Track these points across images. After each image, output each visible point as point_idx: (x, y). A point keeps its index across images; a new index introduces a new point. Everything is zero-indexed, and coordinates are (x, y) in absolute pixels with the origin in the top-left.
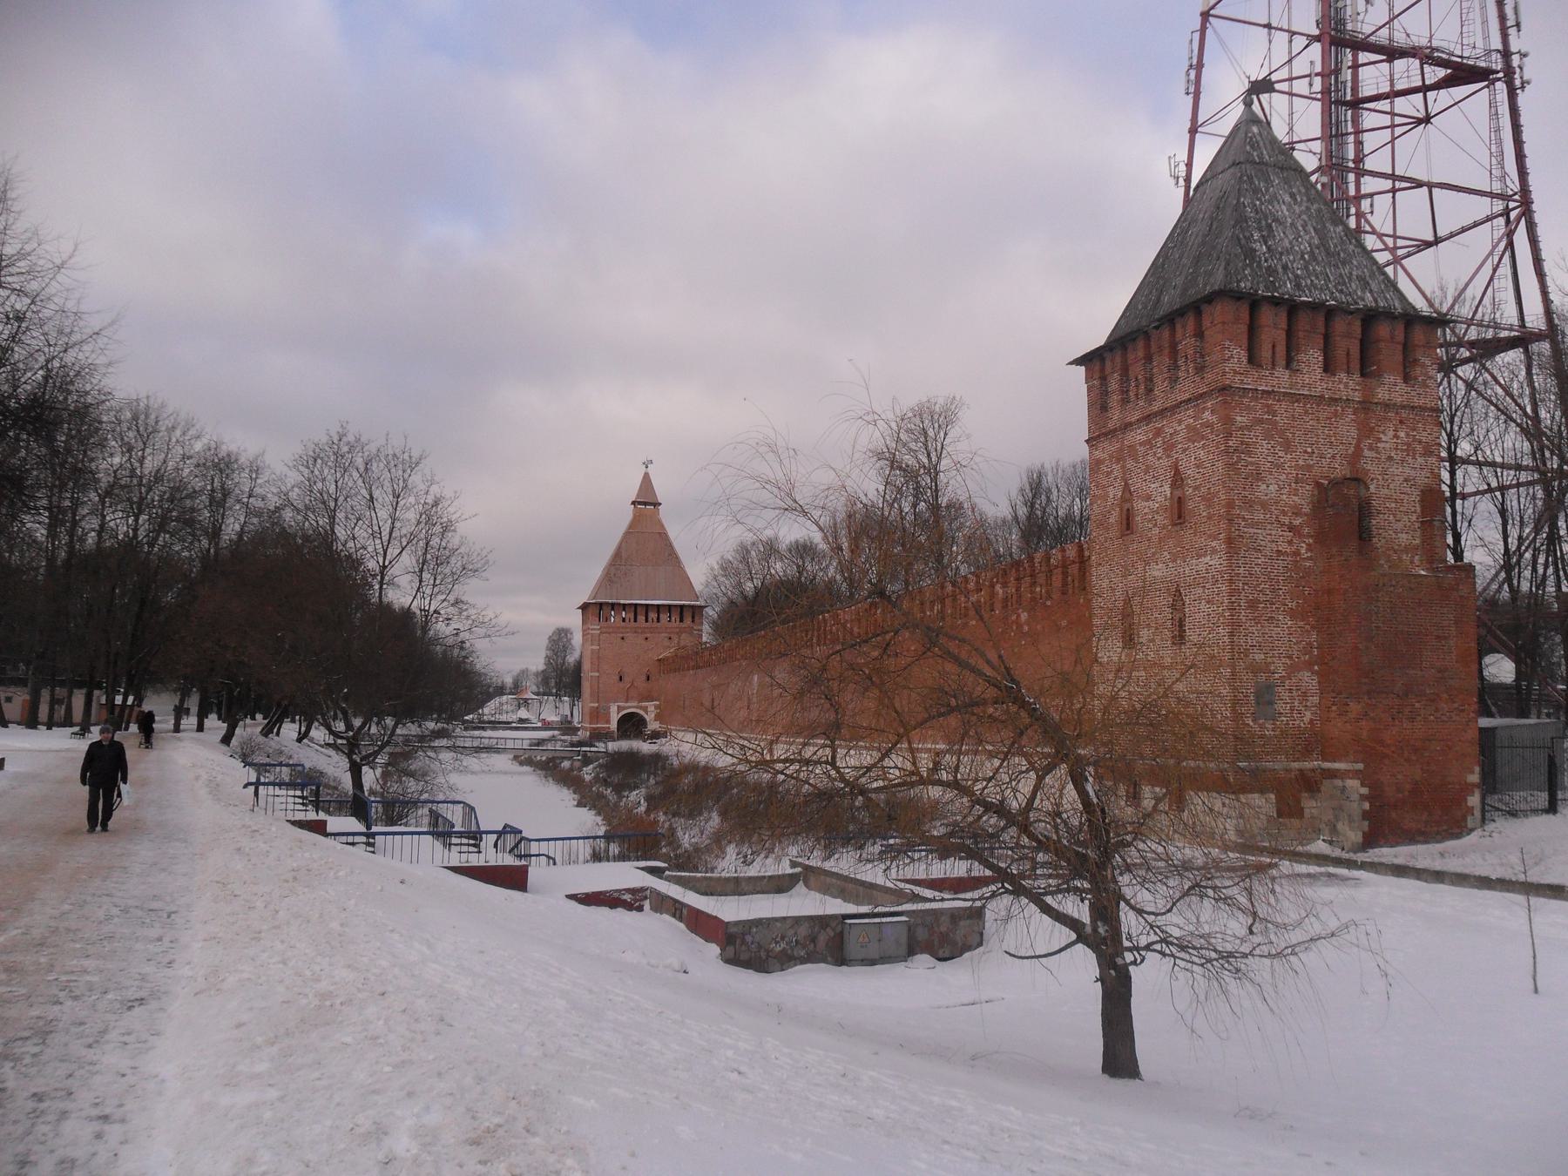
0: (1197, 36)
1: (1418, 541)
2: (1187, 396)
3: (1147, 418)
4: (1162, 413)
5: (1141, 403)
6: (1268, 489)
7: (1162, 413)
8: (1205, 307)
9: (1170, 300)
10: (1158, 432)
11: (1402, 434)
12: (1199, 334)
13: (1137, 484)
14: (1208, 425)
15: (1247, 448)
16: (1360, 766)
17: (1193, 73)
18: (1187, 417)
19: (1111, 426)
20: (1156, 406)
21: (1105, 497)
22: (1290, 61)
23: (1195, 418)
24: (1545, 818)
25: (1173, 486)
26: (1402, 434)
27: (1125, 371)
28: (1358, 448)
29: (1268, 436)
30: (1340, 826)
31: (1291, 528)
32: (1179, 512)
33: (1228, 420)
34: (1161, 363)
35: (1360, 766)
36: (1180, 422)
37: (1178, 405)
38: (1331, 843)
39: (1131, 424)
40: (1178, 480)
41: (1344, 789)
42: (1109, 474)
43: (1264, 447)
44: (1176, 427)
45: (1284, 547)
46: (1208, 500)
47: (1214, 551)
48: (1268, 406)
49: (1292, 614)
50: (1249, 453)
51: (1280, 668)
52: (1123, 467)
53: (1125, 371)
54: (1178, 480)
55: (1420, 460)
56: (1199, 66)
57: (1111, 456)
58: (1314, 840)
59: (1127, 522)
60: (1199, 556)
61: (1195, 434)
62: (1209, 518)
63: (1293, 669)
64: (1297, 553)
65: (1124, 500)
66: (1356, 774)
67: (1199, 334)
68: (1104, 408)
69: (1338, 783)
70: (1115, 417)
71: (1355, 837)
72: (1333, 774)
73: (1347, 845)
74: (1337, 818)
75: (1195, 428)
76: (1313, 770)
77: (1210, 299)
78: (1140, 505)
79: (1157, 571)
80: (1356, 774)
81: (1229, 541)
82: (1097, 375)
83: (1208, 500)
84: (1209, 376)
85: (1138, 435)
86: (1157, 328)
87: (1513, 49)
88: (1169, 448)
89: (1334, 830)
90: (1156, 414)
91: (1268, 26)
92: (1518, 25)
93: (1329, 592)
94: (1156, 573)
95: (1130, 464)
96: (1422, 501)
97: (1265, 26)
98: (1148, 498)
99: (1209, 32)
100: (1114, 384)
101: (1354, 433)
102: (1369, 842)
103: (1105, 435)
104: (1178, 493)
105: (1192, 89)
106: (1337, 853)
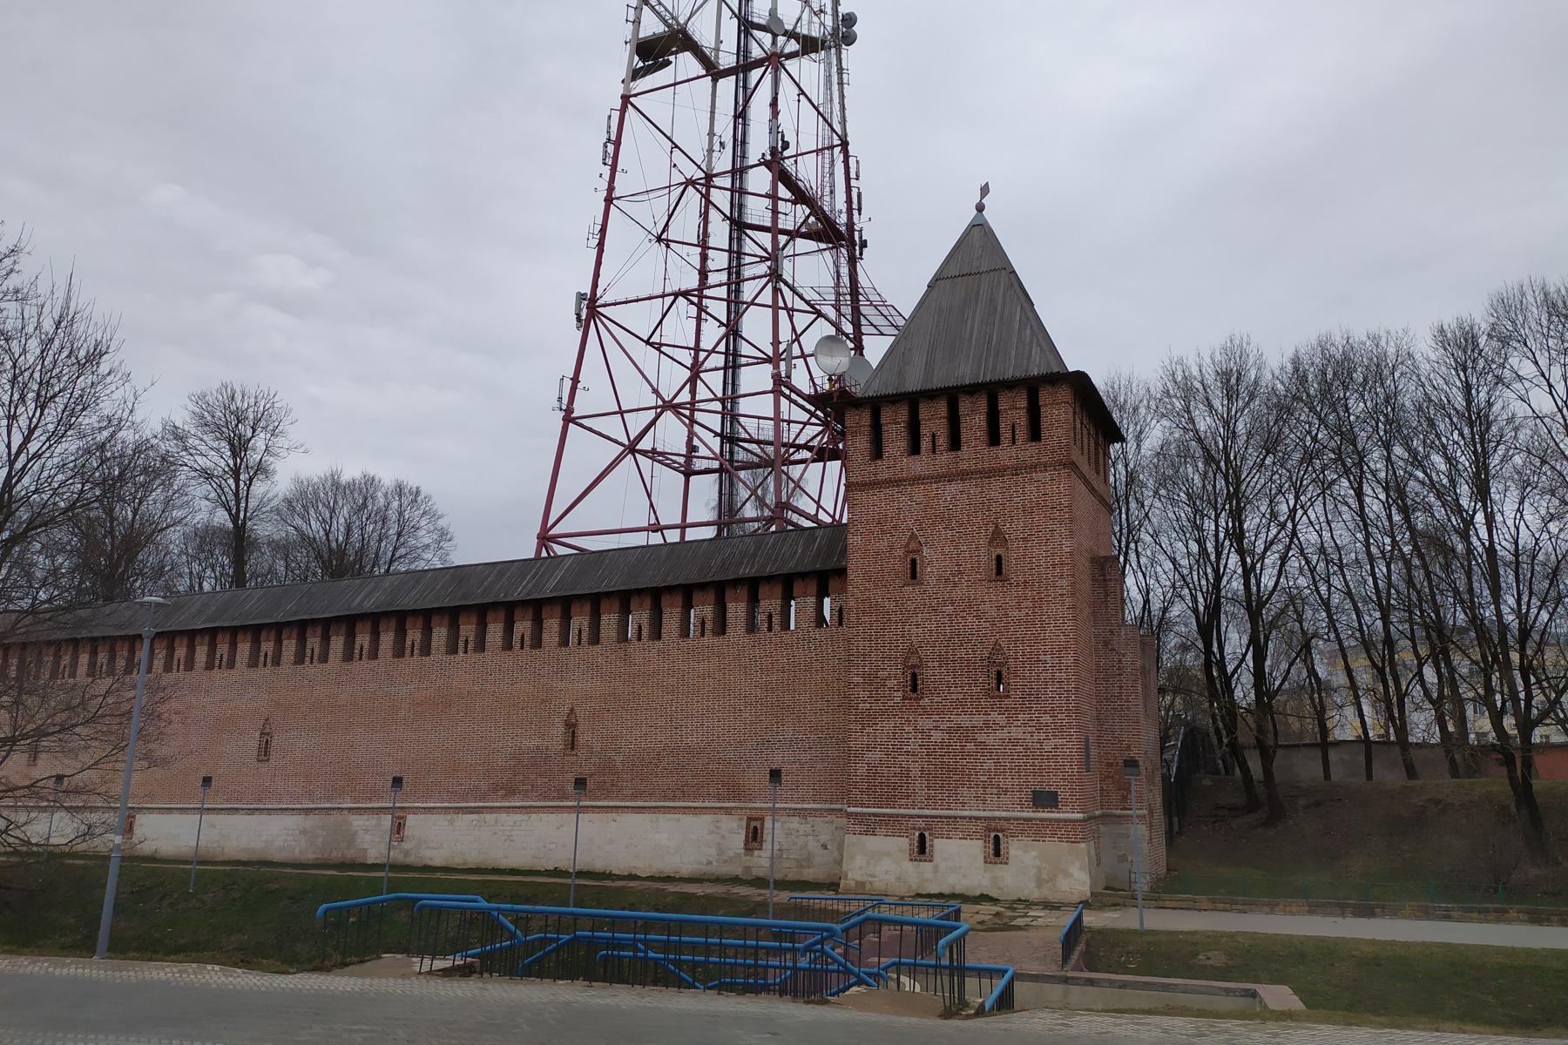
0: (616, 116)
17: (611, 148)
56: (617, 144)
92: (860, 210)
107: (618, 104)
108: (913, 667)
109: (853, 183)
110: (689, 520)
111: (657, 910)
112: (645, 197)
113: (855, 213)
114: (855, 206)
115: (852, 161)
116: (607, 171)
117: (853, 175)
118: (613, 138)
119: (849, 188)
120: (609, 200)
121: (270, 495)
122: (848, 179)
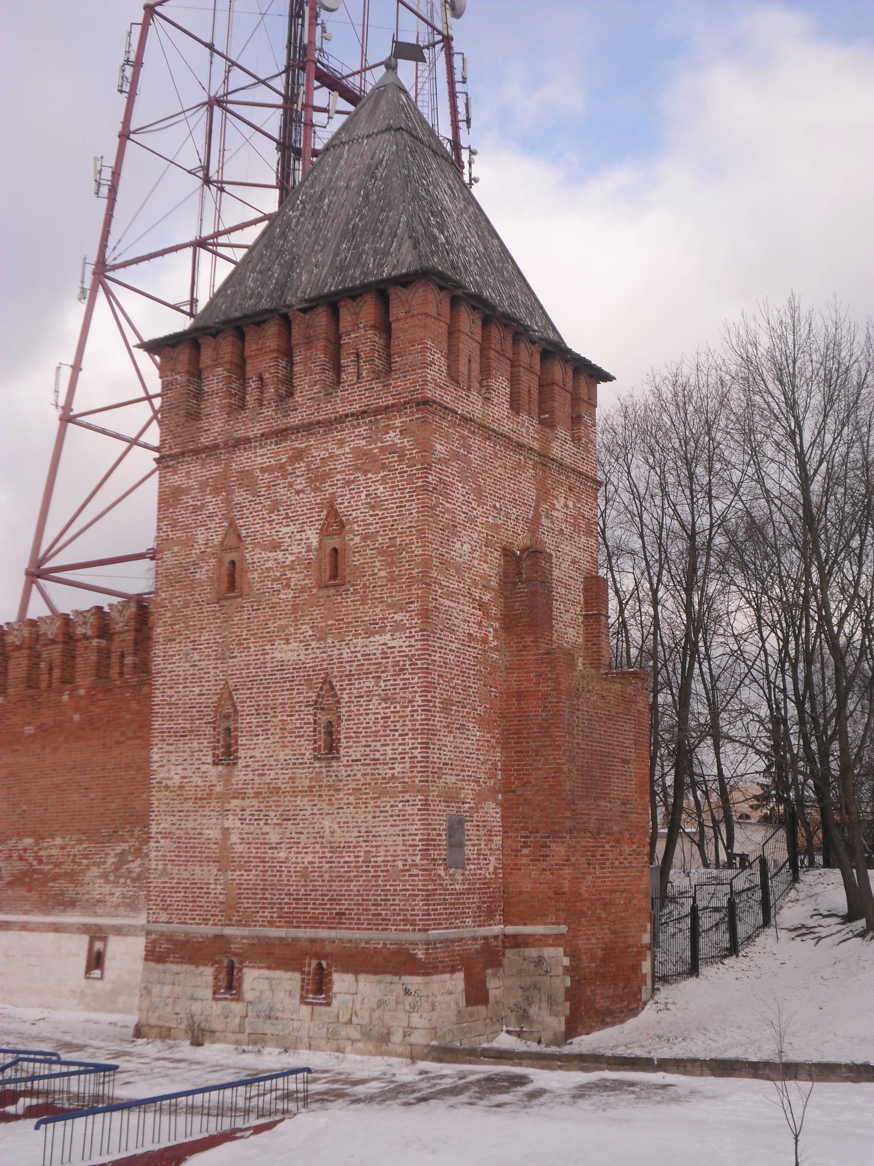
0: (137, 30)
1: (581, 640)
2: (356, 407)
3: (282, 434)
4: (308, 428)
5: (268, 412)
6: (462, 549)
7: (308, 428)
8: (396, 294)
9: (313, 276)
10: (298, 456)
11: (571, 504)
12: (385, 328)
13: (252, 524)
14: (392, 449)
15: (443, 488)
16: (564, 929)
17: (129, 71)
18: (356, 437)
19: (205, 440)
20: (296, 419)
21: (189, 542)
22: (264, 82)
23: (370, 439)
24: (692, 982)
25: (324, 533)
26: (571, 504)
27: (240, 368)
28: (537, 515)
29: (464, 480)
30: (533, 1011)
31: (482, 606)
32: (334, 569)
33: (425, 447)
34: (310, 365)
35: (564, 929)
36: (341, 443)
37: (341, 419)
38: (519, 1035)
39: (247, 440)
40: (334, 522)
41: (540, 961)
42: (196, 509)
43: (459, 491)
44: (339, 450)
45: (474, 630)
46: (391, 554)
47: (398, 627)
48: (464, 438)
49: (481, 722)
50: (447, 496)
51: (468, 792)
52: (228, 501)
53: (240, 368)
54: (334, 522)
55: (583, 539)
56: (138, 65)
57: (203, 486)
58: (496, 1033)
59: (232, 580)
60: (369, 634)
61: (366, 462)
62: (391, 579)
63: (481, 798)
64: (485, 641)
65: (225, 548)
66: (556, 940)
67: (385, 328)
68: (194, 416)
69: (533, 952)
70: (215, 426)
71: (558, 1024)
72: (518, 942)
73: (547, 1036)
74: (529, 1001)
75: (367, 454)
76: (496, 937)
77: (405, 281)
78: (254, 556)
79: (287, 653)
80: (556, 940)
81: (425, 614)
82: (183, 367)
83: (391, 554)
84: (399, 384)
85: (261, 457)
86: (304, 311)
87: (463, 143)
88: (318, 479)
89: (524, 1016)
90: (296, 429)
91: (210, 46)
92: (468, 121)
93: (520, 695)
94: (285, 656)
95: (240, 496)
96: (586, 590)
97: (206, 45)
98: (275, 546)
99: (151, 29)
100: (215, 380)
101: (533, 493)
102: (572, 1030)
103: (196, 452)
104: (332, 542)
105: (127, 88)
106: (534, 1047)
107: (140, 16)
108: (227, 717)
109: (459, 87)
110: (127, 444)
111: (289, 924)
112: (182, 117)
113: (463, 125)
114: (462, 116)
115: (457, 61)
116: (123, 99)
117: (458, 77)
118: (132, 57)
119: (453, 95)
120: (125, 135)
121: (775, 324)
122: (451, 83)
